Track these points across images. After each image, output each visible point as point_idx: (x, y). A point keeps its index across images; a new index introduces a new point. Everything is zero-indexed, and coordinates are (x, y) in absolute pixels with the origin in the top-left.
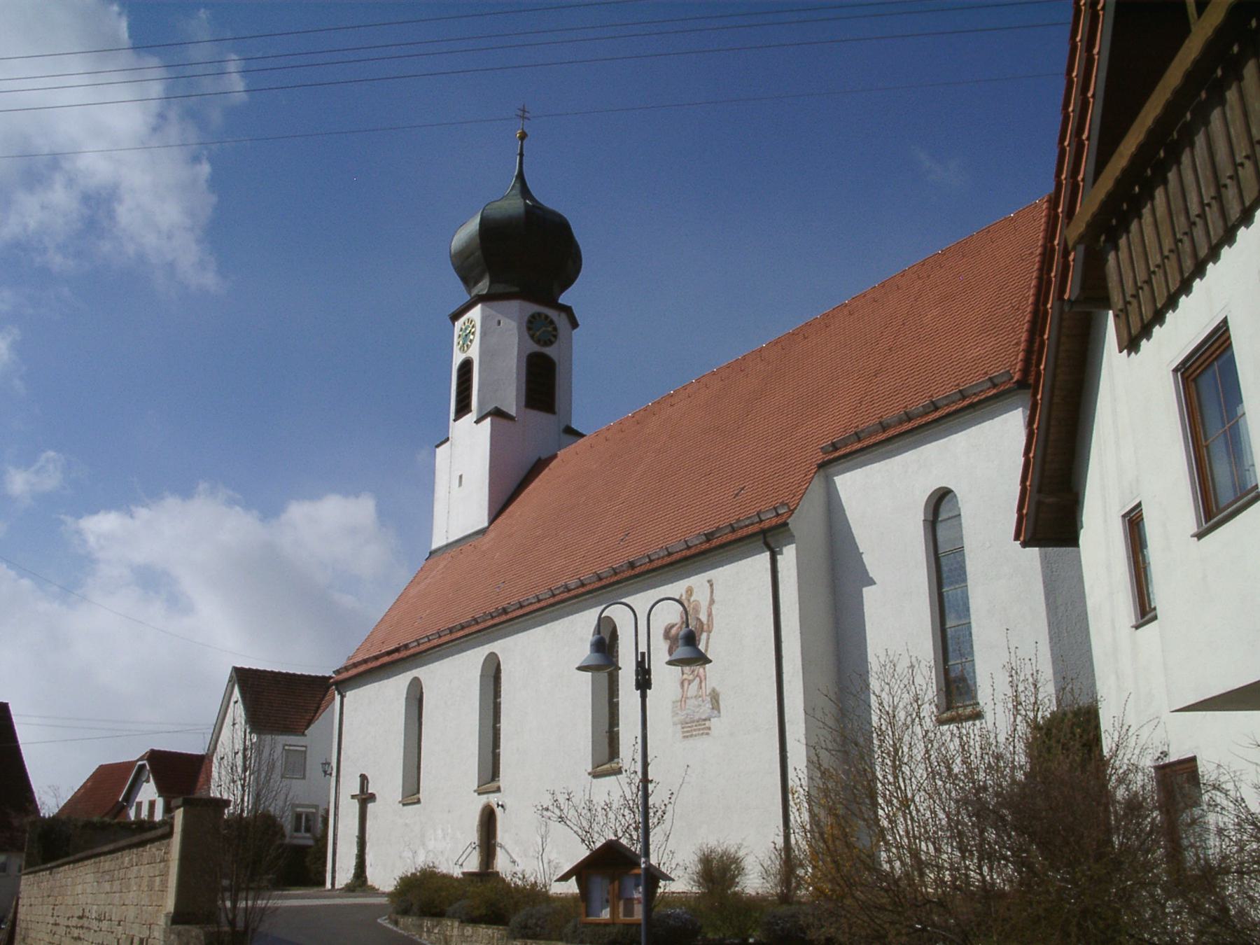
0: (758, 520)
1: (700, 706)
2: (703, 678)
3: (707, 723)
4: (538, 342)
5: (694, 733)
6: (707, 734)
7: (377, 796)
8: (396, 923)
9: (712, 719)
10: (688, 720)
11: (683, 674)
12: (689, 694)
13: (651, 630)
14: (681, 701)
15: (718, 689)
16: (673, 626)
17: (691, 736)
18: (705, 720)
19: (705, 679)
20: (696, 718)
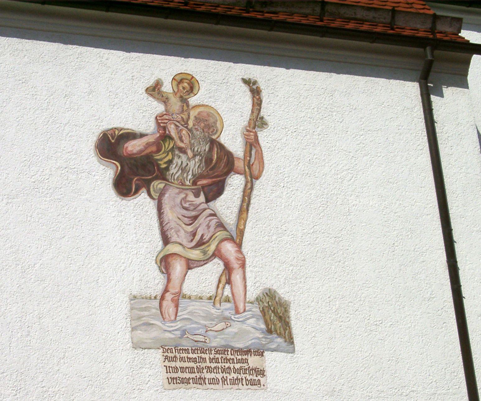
0: (388, 20)
1: (226, 319)
2: (235, 264)
3: (253, 361)
4: (253, 82)
5: (208, 376)
6: (253, 383)
7: (93, 139)
8: (174, 164)
9: (266, 353)
10: (186, 344)
11: (166, 240)
12: (187, 289)
13: (422, 125)
14: (163, 298)
15: (283, 293)
16: (131, 136)
17: (200, 381)
18: (248, 352)
19: (243, 266)
20: (215, 343)
